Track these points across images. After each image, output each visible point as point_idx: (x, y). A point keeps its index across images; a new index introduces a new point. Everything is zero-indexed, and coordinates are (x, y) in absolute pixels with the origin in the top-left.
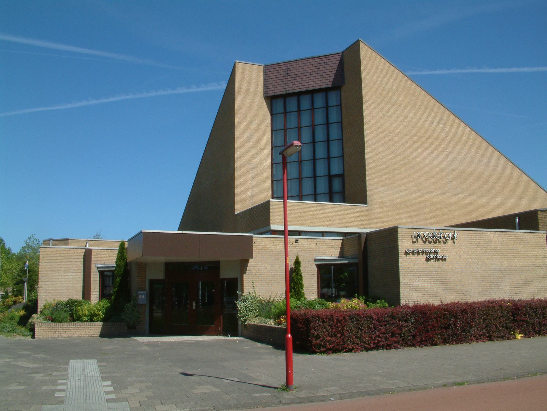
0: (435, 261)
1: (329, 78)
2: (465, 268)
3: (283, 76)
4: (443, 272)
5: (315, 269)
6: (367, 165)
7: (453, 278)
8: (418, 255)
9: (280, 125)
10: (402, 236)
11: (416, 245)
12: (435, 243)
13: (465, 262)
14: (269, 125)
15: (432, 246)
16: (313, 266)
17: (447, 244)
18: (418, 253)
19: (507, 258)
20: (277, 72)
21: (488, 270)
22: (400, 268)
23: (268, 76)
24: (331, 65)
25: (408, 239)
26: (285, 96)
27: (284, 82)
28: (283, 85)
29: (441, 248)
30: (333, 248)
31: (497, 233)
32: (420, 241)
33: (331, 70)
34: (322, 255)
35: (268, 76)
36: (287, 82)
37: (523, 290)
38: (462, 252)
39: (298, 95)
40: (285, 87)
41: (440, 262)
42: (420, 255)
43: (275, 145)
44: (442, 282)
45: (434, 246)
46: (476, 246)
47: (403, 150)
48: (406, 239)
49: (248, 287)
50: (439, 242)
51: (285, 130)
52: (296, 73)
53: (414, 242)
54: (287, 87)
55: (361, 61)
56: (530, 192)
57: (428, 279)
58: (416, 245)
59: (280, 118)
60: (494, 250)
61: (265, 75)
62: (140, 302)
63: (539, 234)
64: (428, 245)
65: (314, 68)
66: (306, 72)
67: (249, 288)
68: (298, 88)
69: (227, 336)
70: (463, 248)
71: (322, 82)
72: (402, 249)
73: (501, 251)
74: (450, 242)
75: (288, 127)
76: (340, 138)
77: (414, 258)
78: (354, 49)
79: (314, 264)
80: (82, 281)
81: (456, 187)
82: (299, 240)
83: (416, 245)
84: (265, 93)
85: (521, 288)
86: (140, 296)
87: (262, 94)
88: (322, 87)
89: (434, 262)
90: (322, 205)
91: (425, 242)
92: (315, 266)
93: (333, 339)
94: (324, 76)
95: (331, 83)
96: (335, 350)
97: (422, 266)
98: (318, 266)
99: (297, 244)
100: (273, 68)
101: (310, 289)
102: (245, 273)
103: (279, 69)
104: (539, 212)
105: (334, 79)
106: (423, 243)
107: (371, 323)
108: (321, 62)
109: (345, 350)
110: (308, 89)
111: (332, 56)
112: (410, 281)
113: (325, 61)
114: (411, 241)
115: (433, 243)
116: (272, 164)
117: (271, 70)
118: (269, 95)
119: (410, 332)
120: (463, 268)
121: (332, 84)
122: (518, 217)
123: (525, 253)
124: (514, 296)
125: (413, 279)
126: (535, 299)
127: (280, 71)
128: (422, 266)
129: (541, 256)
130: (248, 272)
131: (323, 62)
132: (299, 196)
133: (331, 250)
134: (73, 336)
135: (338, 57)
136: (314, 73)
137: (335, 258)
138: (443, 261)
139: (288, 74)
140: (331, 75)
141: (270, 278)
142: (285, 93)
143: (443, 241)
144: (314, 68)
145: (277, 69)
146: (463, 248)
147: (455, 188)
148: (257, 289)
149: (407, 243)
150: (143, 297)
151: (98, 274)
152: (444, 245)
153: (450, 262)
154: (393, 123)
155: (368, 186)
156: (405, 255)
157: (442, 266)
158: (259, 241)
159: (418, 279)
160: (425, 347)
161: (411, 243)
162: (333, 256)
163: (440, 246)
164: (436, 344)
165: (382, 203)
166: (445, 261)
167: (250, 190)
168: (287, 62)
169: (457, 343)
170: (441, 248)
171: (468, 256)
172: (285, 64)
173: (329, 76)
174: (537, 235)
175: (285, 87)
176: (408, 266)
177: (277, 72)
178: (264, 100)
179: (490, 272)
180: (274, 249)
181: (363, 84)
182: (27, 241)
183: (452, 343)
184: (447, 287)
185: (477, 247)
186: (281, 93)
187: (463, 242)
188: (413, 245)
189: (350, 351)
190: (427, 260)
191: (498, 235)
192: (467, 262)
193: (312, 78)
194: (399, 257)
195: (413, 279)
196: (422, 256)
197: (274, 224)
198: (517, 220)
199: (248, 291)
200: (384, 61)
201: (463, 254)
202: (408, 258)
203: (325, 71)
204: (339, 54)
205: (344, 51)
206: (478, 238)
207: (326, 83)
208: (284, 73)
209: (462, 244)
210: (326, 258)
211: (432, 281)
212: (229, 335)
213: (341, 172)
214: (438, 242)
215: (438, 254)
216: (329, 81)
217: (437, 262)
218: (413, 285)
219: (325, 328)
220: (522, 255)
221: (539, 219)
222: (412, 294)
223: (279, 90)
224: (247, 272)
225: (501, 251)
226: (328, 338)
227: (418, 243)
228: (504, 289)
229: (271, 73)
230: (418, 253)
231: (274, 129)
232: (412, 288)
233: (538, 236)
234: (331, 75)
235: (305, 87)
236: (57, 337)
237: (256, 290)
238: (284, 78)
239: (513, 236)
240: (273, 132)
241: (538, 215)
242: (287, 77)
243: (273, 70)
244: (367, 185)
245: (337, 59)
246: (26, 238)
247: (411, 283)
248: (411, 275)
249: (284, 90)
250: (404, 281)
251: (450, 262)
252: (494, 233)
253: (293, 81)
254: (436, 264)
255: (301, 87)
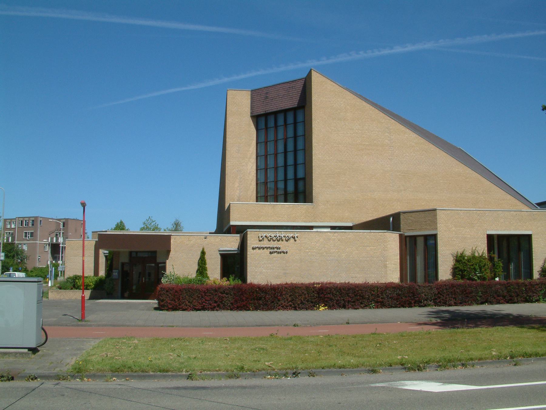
0: (278, 254)
1: (295, 100)
2: (304, 259)
3: (263, 98)
4: (285, 262)
5: (219, 257)
6: (313, 171)
7: (293, 266)
8: (263, 249)
9: (263, 139)
10: (250, 237)
11: (262, 242)
12: (278, 241)
13: (304, 254)
14: (255, 139)
15: (275, 243)
16: (217, 255)
17: (289, 241)
18: (263, 248)
19: (345, 252)
20: (260, 95)
21: (326, 260)
22: (248, 259)
23: (254, 99)
24: (297, 89)
25: (256, 238)
26: (266, 115)
27: (265, 104)
28: (264, 106)
29: (283, 245)
30: (234, 242)
31: (336, 233)
32: (266, 239)
33: (297, 93)
34: (224, 247)
35: (254, 99)
36: (266, 104)
37: (359, 276)
38: (302, 247)
39: (275, 114)
40: (265, 108)
41: (282, 254)
42: (265, 250)
43: (259, 155)
44: (283, 269)
45: (277, 243)
46: (316, 243)
47: (348, 157)
48: (254, 238)
49: (169, 269)
50: (282, 240)
51: (266, 143)
52: (273, 96)
53: (260, 241)
54: (266, 108)
55: (313, 86)
56: (479, 186)
57: (271, 266)
58: (262, 243)
59: (263, 133)
60: (333, 246)
61: (252, 98)
62: (114, 277)
63: (379, 233)
64: (272, 243)
65: (285, 91)
66: (279, 95)
67: (170, 269)
68: (274, 108)
69: (154, 300)
70: (303, 244)
71: (290, 103)
72: (440, 234)
73: (340, 246)
74: (292, 240)
75: (269, 140)
76: (304, 148)
77: (260, 251)
78: (309, 75)
79: (218, 253)
80: (94, 263)
81: (399, 186)
82: (208, 237)
83: (262, 243)
84: (251, 113)
85: (358, 274)
86: (114, 273)
87: (249, 114)
88: (291, 107)
89: (277, 254)
90: (273, 205)
91: (269, 241)
92: (219, 255)
93: (173, 302)
94: (292, 98)
95: (297, 103)
96: (175, 309)
97: (266, 257)
98: (221, 255)
99: (205, 239)
100: (257, 92)
101: (215, 270)
102: (168, 259)
103: (261, 93)
104: (401, 214)
105: (299, 100)
106: (268, 241)
107: (199, 294)
108: (290, 86)
109: (181, 309)
110: (280, 109)
111: (298, 81)
112: (256, 267)
113: (293, 86)
114: (258, 240)
115: (276, 241)
116: (257, 170)
117: (256, 94)
118: (254, 114)
119: (229, 301)
120: (302, 259)
121: (298, 104)
122: (392, 217)
123: (363, 247)
124: (350, 280)
125: (259, 266)
126: (325, 282)
127: (261, 95)
128: (266, 257)
129: (380, 250)
130: (169, 258)
131: (291, 86)
132: (264, 196)
133: (232, 244)
134: (72, 298)
135: (302, 82)
136: (285, 96)
137: (235, 249)
138: (284, 254)
139: (267, 97)
140: (296, 97)
141: (186, 262)
142: (265, 112)
143: (286, 239)
144: (285, 91)
145: (260, 93)
146: (303, 244)
147: (398, 186)
148: (176, 270)
149: (254, 241)
150: (116, 274)
151: (104, 258)
152: (286, 242)
153: (291, 254)
154: (340, 135)
155: (314, 188)
156: (252, 249)
157: (283, 257)
158: (178, 238)
159: (262, 266)
160: (223, 311)
161: (258, 241)
162: (233, 247)
163: (283, 243)
164: (249, 310)
165: (326, 202)
166: (287, 253)
167: (238, 191)
168: (267, 87)
169: (266, 310)
170: (283, 245)
171: (308, 250)
172: (265, 88)
173: (295, 98)
174: (378, 233)
175: (265, 108)
176: (254, 257)
177: (260, 95)
178: (251, 119)
179: (327, 262)
180: (189, 243)
181: (313, 105)
182: (145, 222)
183: (263, 309)
184: (287, 272)
185: (317, 244)
186: (262, 113)
187: (303, 240)
188: (260, 242)
189: (184, 310)
190: (271, 253)
191: (337, 235)
192: (306, 254)
193: (283, 100)
194: (247, 251)
195: (259, 266)
196: (267, 250)
197: (233, 221)
198: (391, 219)
199: (170, 271)
200: (334, 84)
201: (303, 249)
202: (255, 251)
203: (293, 94)
204: (303, 80)
205: (306, 77)
206: (317, 237)
207: (290, 105)
208: (265, 96)
209: (302, 242)
210: (227, 249)
211: (275, 267)
212: (156, 300)
213: (304, 177)
214: (281, 240)
215: (281, 249)
216: (295, 102)
217: (279, 254)
218: (258, 270)
219: (168, 295)
220: (360, 249)
221: (401, 219)
222: (257, 276)
223: (261, 111)
224: (169, 258)
225: (340, 246)
226: (169, 301)
227: (264, 241)
228: (340, 274)
229: (255, 96)
230: (263, 248)
231: (260, 141)
232: (257, 272)
233: (378, 235)
234: (296, 97)
235: (279, 107)
236: (62, 299)
237: (175, 270)
238: (265, 100)
239: (352, 235)
240: (259, 144)
241: (401, 216)
242: (266, 100)
243: (257, 94)
244: (313, 187)
245: (301, 84)
246: (144, 220)
247: (256, 269)
248: (257, 263)
249: (264, 110)
250: (250, 267)
251: (291, 254)
252: (334, 233)
253: (271, 103)
254: (278, 256)
255: (276, 108)
